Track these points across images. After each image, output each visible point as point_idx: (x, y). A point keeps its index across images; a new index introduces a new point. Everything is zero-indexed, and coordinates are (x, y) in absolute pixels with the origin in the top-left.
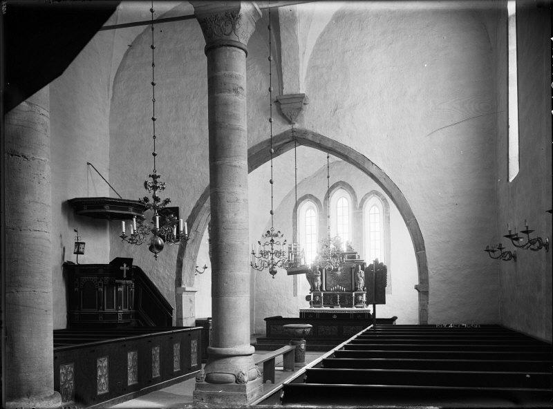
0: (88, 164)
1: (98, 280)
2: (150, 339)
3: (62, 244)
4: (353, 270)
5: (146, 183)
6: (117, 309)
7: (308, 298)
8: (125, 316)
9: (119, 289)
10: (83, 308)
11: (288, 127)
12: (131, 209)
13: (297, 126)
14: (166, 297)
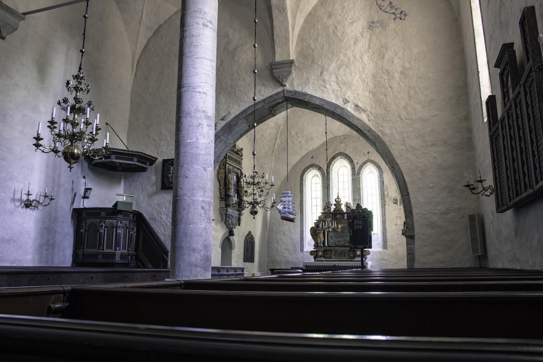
0: (107, 124)
1: (101, 222)
2: (127, 274)
3: (73, 189)
5: (68, 83)
6: (116, 250)
7: (312, 253)
8: (122, 256)
9: (118, 231)
10: (87, 248)
11: (280, 89)
12: (136, 160)
13: (288, 87)
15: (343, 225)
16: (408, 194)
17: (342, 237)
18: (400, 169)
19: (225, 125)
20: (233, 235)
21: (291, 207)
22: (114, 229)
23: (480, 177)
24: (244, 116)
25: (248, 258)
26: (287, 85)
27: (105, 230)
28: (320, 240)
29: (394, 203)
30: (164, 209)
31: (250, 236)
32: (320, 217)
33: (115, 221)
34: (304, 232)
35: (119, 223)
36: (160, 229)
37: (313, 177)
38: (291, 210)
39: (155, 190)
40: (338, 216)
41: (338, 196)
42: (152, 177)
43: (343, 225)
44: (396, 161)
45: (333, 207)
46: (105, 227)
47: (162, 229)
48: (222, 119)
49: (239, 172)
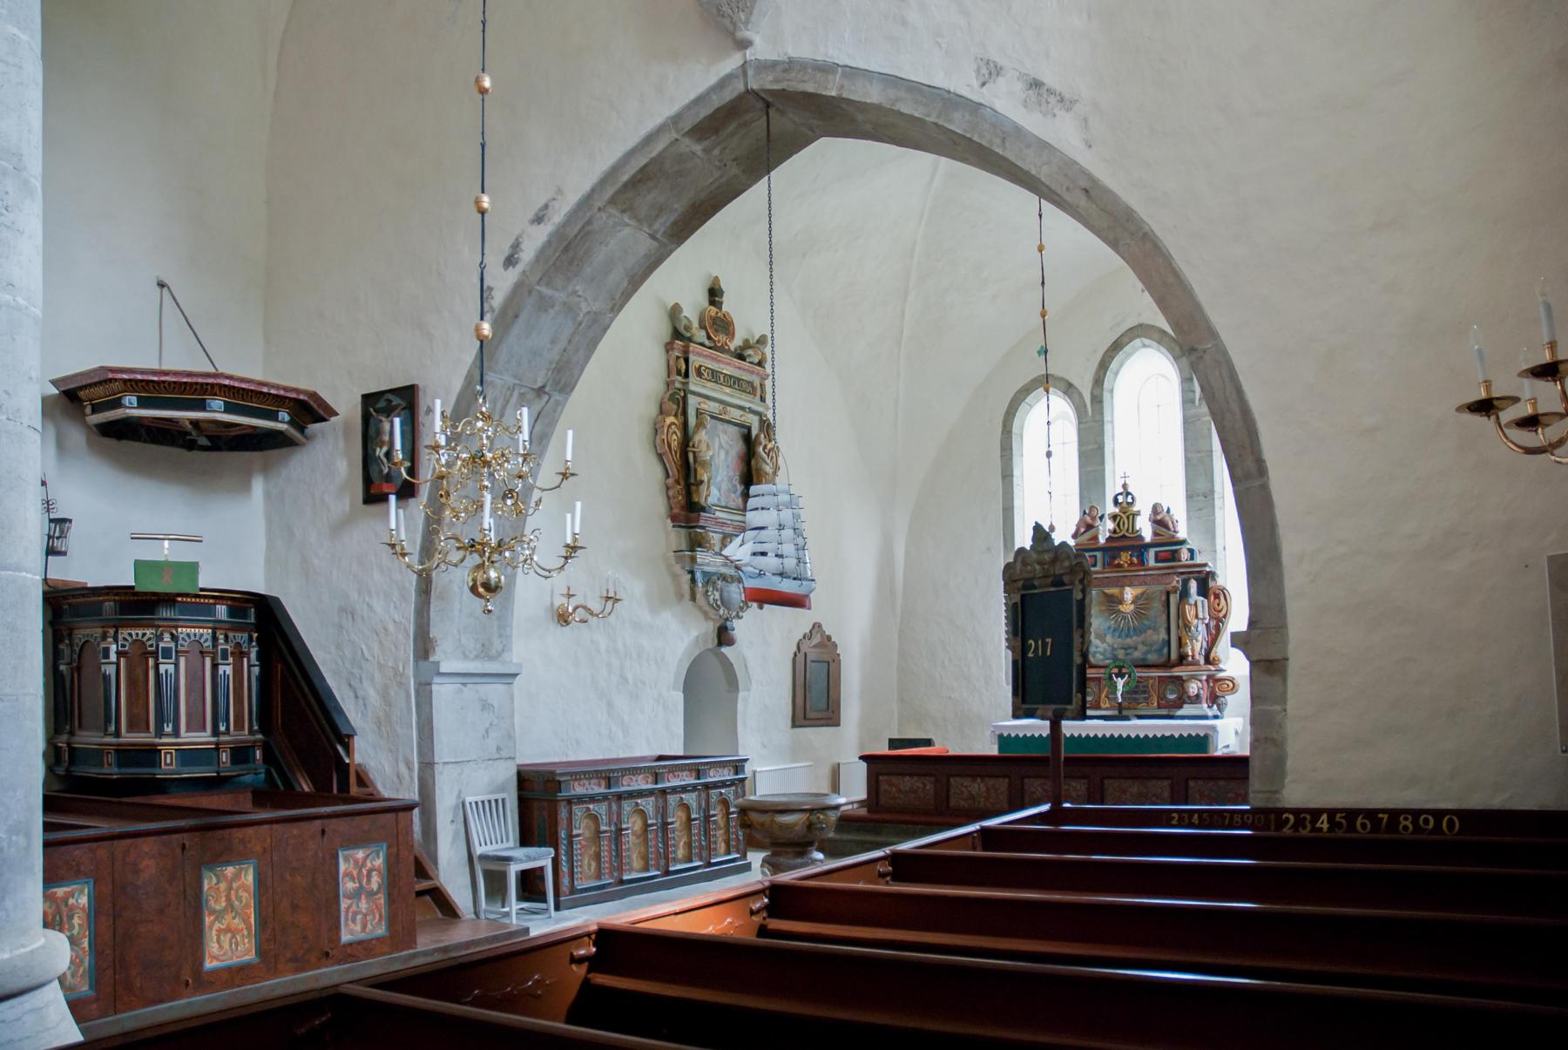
0: (162, 285)
4: (1174, 599)
6: (160, 732)
9: (162, 668)
11: (732, 63)
12: (134, 400)
13: (762, 49)
14: (331, 682)
15: (1139, 590)
16: (1262, 470)
17: (1139, 631)
18: (1225, 353)
19: (549, 243)
20: (730, 642)
21: (788, 549)
22: (151, 662)
23: (1552, 346)
24: (609, 192)
25: (811, 715)
26: (758, 40)
27: (118, 665)
30: (377, 576)
31: (817, 639)
33: (149, 632)
35: (167, 637)
36: (369, 648)
38: (790, 563)
39: (347, 508)
40: (1125, 557)
41: (1125, 486)
42: (331, 458)
43: (1139, 590)
44: (1207, 321)
45: (1106, 528)
46: (119, 654)
47: (376, 646)
48: (538, 219)
49: (754, 422)
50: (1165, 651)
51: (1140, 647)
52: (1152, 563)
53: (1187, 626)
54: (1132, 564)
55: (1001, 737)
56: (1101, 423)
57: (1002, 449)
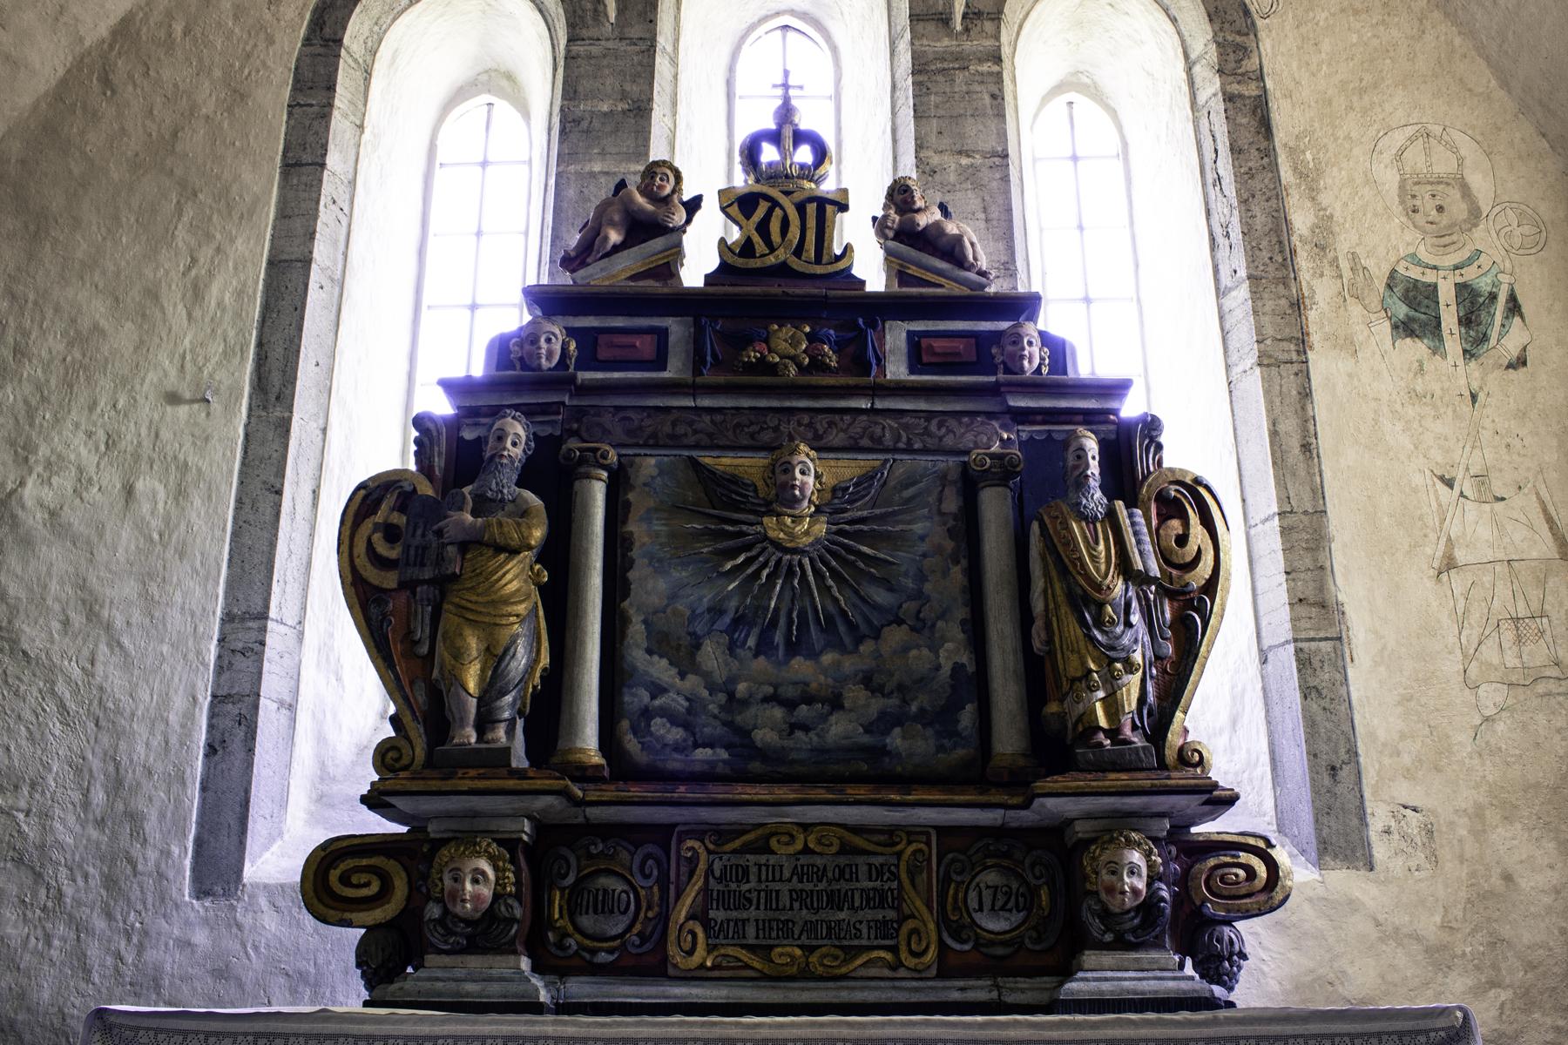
4: (995, 506)
15: (848, 468)
17: (846, 631)
28: (496, 658)
29: (1405, 328)
32: (512, 356)
34: (276, 638)
37: (460, 94)
40: (788, 342)
43: (848, 468)
50: (967, 718)
51: (855, 695)
52: (897, 369)
53: (1086, 600)
54: (818, 365)
55: (364, 800)
56: (649, 47)
57: (300, 84)
